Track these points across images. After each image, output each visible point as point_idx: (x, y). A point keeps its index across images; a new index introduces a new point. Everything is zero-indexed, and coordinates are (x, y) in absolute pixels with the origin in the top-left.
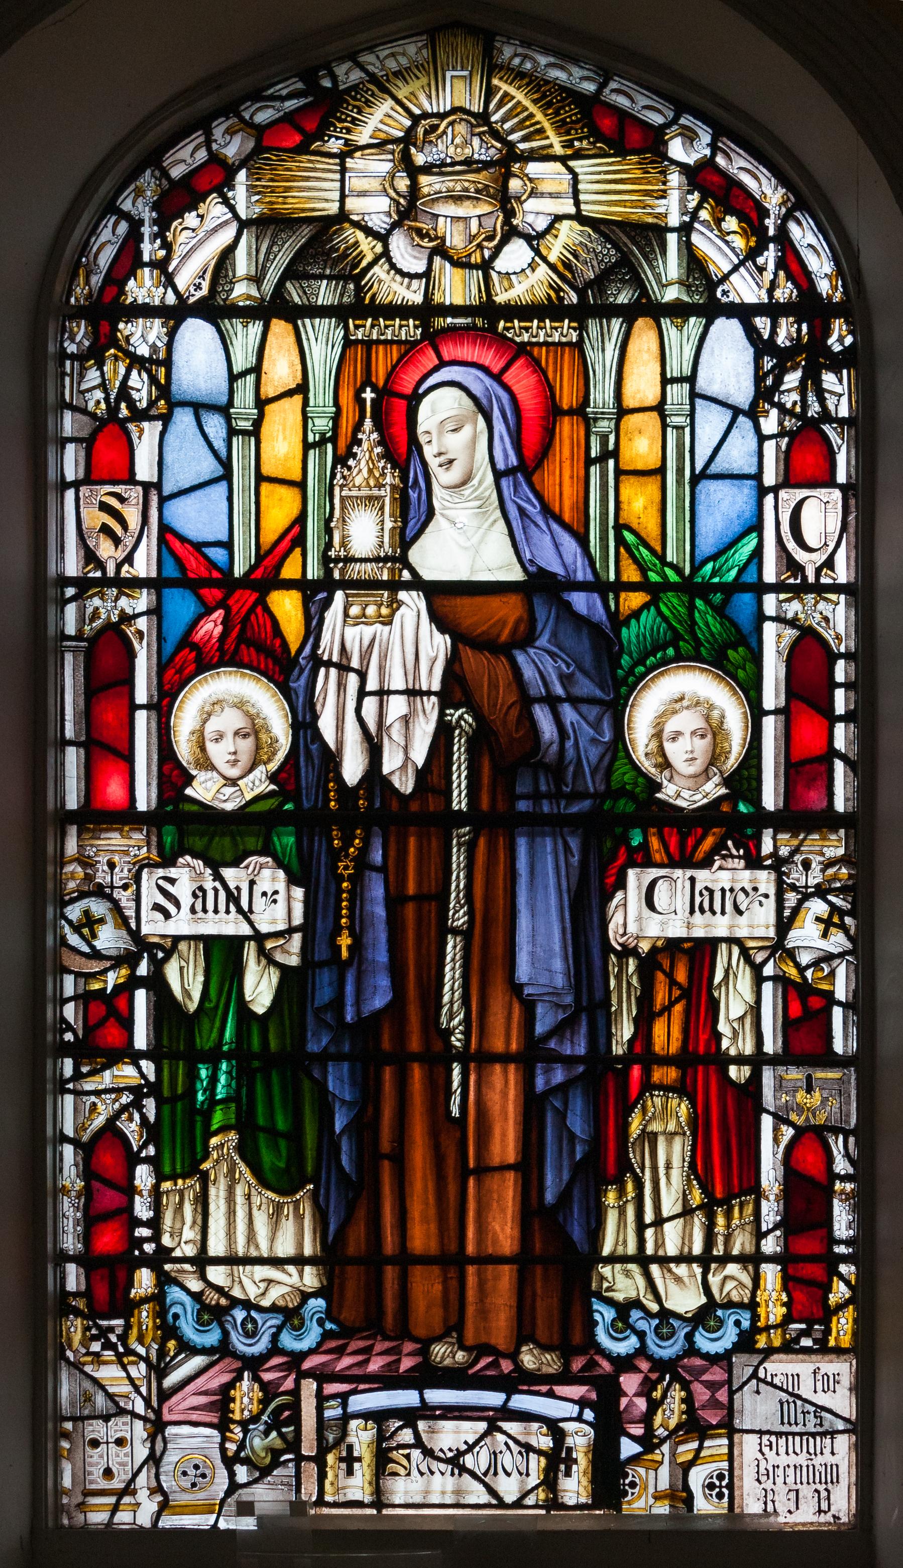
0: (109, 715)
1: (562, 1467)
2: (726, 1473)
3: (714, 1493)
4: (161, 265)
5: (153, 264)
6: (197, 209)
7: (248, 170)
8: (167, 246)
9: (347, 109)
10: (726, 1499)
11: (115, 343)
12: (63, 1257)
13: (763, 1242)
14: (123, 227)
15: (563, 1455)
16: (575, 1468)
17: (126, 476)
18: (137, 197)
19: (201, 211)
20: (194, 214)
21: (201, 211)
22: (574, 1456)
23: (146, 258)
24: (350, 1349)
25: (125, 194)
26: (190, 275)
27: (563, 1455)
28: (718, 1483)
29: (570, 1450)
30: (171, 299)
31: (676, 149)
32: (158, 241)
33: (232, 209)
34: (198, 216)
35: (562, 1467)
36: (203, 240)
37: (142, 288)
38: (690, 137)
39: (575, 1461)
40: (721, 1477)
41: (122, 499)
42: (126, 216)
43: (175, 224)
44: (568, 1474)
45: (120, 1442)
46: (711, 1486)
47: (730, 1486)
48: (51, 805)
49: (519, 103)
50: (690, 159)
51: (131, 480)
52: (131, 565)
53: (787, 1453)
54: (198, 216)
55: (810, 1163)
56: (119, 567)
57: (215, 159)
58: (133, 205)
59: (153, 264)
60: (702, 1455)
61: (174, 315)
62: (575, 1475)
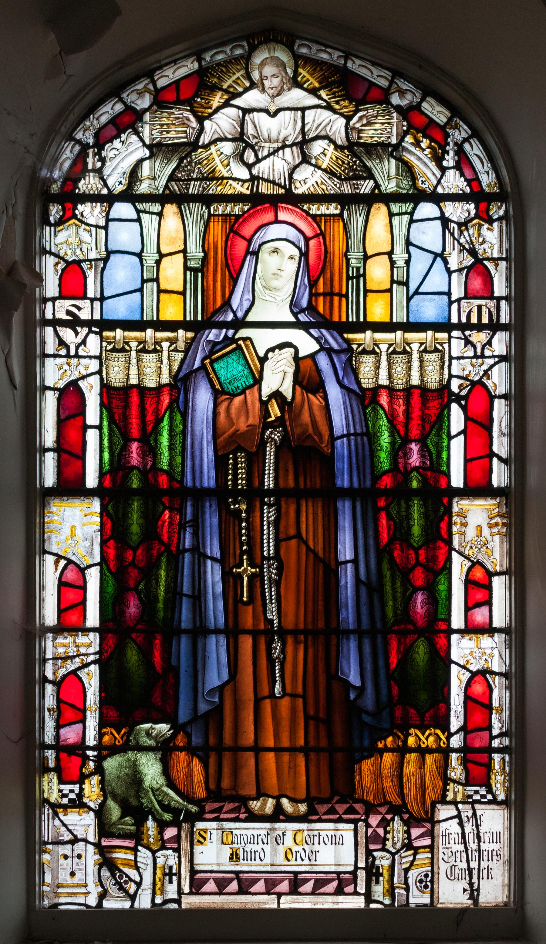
0: (72, 435)
1: (374, 878)
2: (430, 873)
3: (422, 885)
4: (99, 172)
5: (94, 170)
6: (120, 137)
7: (151, 113)
8: (103, 160)
9: (205, 95)
10: (429, 889)
11: (75, 216)
12: (45, 747)
13: (452, 739)
14: (77, 148)
15: (374, 871)
16: (381, 878)
17: (82, 295)
18: (85, 130)
19: (122, 139)
20: (118, 140)
21: (122, 139)
22: (381, 871)
23: (90, 167)
24: (225, 809)
25: (79, 129)
26: (116, 180)
27: (374, 871)
28: (425, 880)
29: (378, 868)
30: (105, 191)
31: (395, 99)
32: (97, 157)
33: (142, 140)
34: (121, 141)
35: (374, 878)
36: (124, 156)
37: (89, 184)
38: (402, 93)
39: (382, 875)
40: (426, 876)
41: (79, 309)
42: (79, 142)
43: (107, 146)
44: (377, 882)
45: (79, 856)
46: (421, 881)
47: (432, 881)
48: (38, 486)
49: (304, 77)
50: (404, 103)
51: (84, 297)
52: (85, 346)
53: (488, 860)
54: (121, 141)
55: (478, 689)
56: (77, 348)
57: (129, 109)
58: (83, 135)
59: (94, 170)
60: (415, 863)
61: (110, 199)
62: (381, 883)
